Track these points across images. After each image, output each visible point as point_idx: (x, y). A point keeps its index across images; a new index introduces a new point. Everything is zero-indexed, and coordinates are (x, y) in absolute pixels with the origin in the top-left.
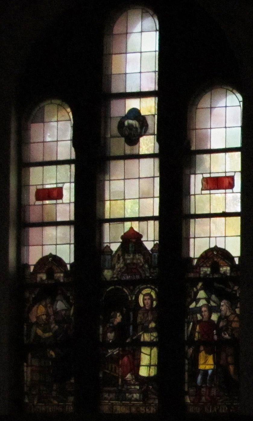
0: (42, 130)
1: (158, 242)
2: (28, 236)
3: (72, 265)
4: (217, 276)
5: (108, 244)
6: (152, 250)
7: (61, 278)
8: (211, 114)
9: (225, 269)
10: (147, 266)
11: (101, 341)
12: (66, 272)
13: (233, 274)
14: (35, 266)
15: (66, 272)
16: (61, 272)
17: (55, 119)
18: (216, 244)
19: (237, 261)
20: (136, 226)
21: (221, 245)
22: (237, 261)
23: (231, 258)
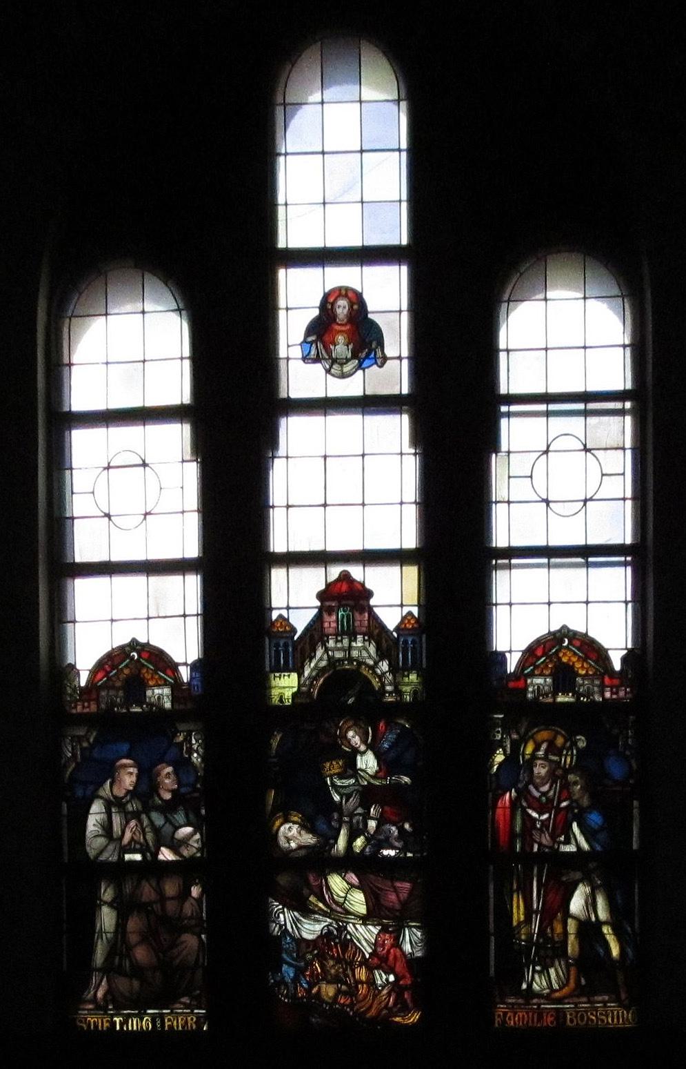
0: (284, 141)
1: (415, 611)
2: (179, 574)
3: (194, 667)
4: (139, 710)
5: (284, 613)
6: (398, 629)
7: (166, 699)
8: (596, 297)
9: (161, 694)
10: (384, 666)
11: (66, 861)
12: (176, 686)
13: (176, 707)
14: (94, 672)
15: (176, 686)
16: (166, 684)
17: (316, 97)
18: (79, 622)
19: (185, 673)
20: (356, 572)
21: (578, 626)
22: (185, 673)
23: (173, 667)
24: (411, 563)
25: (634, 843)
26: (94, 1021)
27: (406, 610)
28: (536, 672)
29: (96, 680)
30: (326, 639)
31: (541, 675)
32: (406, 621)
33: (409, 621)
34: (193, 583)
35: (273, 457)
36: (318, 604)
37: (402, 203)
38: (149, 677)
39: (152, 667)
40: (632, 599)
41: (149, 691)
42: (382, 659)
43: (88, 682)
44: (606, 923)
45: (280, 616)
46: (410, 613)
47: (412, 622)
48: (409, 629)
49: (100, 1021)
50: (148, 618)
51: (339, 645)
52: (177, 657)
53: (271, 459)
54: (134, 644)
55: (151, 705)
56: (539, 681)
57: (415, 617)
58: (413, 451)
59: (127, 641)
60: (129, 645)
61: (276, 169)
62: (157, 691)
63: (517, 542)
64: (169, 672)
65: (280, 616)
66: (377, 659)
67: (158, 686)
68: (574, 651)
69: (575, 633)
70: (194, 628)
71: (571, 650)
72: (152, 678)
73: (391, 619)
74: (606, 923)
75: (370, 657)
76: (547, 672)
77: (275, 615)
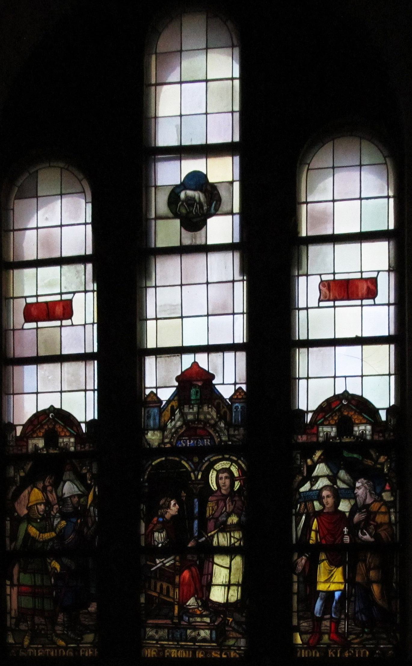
1: (244, 387)
6: (231, 398)
16: (71, 435)
20: (202, 360)
24: (89, 262)
25: (314, 526)
26: (49, 651)
27: (237, 386)
28: (325, 423)
29: (27, 432)
30: (182, 407)
31: (329, 425)
32: (238, 394)
33: (240, 394)
34: (93, 368)
35: (146, 287)
36: (176, 384)
37: (234, 114)
38: (61, 430)
39: (62, 424)
40: (395, 372)
41: (61, 439)
42: (355, 480)
43: (21, 433)
44: (8, 585)
45: (152, 392)
46: (240, 388)
47: (243, 394)
48: (240, 399)
49: (35, 651)
50: (61, 392)
51: (191, 411)
52: (80, 417)
53: (145, 289)
54: (52, 409)
55: (61, 449)
56: (327, 429)
57: (244, 391)
58: (241, 278)
59: (47, 406)
60: (49, 409)
61: (211, 157)
62: (66, 440)
63: (313, 336)
64: (75, 428)
65: (152, 392)
66: (217, 420)
67: (65, 436)
68: (367, 419)
69: (354, 396)
70: (92, 398)
71: (339, 404)
72: (63, 431)
73: (227, 392)
74: (8, 585)
75: (212, 418)
76: (333, 422)
77: (148, 392)
